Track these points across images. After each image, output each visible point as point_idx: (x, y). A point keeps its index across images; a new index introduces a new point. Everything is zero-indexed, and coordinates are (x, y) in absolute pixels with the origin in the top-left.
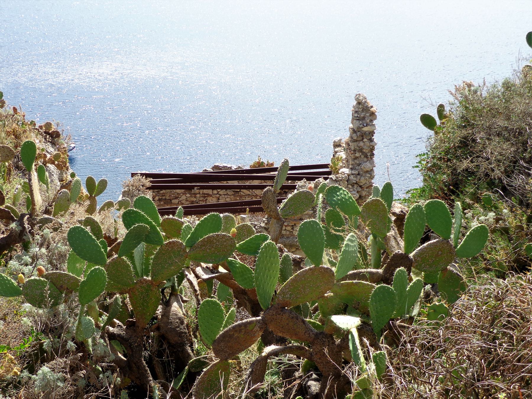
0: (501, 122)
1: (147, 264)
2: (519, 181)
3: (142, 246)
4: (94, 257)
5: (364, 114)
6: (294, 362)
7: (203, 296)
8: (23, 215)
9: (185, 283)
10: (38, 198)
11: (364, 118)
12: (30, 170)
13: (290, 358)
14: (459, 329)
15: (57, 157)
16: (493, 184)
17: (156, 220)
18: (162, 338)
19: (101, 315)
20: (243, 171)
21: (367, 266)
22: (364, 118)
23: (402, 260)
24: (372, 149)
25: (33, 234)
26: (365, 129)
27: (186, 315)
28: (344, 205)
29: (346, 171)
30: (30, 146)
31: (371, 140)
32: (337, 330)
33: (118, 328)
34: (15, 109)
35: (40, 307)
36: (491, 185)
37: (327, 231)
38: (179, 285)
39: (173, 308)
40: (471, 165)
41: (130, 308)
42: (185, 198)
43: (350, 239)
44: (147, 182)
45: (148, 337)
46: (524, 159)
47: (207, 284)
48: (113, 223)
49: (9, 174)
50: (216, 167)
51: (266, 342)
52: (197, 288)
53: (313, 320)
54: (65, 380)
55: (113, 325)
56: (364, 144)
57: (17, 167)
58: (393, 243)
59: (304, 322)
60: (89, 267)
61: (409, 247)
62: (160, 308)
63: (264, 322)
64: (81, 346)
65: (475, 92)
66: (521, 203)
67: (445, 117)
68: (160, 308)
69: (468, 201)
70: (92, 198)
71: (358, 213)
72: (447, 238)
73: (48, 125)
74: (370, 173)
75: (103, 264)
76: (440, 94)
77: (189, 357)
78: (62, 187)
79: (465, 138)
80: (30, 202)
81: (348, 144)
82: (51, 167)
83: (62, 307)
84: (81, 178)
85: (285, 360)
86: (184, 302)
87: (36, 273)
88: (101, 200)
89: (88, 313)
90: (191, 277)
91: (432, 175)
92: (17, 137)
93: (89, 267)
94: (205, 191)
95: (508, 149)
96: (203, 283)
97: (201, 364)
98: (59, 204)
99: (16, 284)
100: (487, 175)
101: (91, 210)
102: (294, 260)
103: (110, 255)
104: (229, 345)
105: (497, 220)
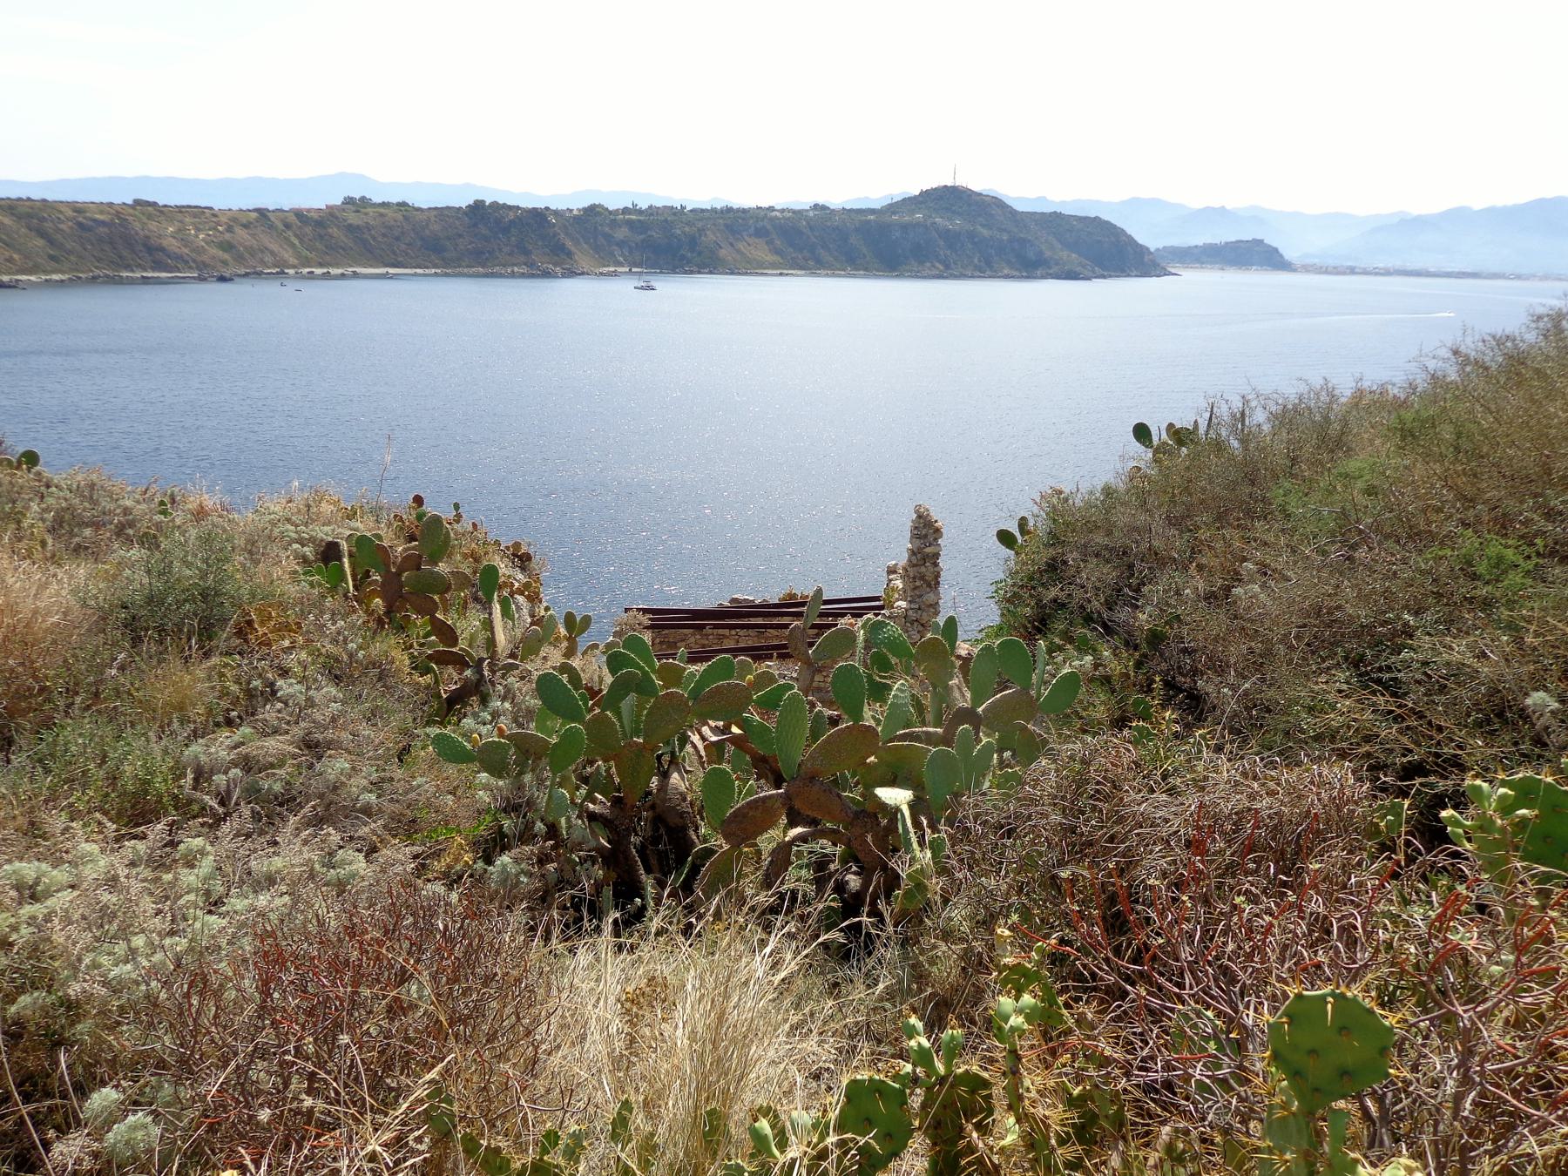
0: (1100, 539)
1: (637, 722)
2: (1122, 614)
3: (631, 698)
4: (572, 714)
5: (926, 531)
6: (828, 851)
7: (709, 763)
8: (481, 660)
9: (689, 748)
10: (501, 638)
11: (926, 536)
12: (490, 601)
13: (825, 846)
14: (1034, 801)
15: (527, 586)
16: (1092, 619)
17: (651, 665)
18: (658, 820)
19: (578, 788)
20: (769, 606)
21: (924, 724)
22: (926, 536)
23: (968, 715)
24: (938, 576)
25: (493, 685)
26: (928, 550)
27: (690, 789)
28: (895, 645)
29: (903, 604)
30: (492, 571)
31: (936, 565)
32: (883, 806)
33: (600, 805)
34: (474, 525)
35: (500, 777)
36: (1088, 620)
37: (869, 677)
38: (681, 750)
39: (672, 781)
40: (1062, 595)
41: (617, 780)
42: (694, 640)
43: (899, 687)
44: (645, 620)
45: (640, 819)
46: (1129, 586)
47: (716, 750)
48: (595, 669)
49: (465, 607)
50: (734, 600)
51: (792, 824)
52: (703, 753)
53: (855, 795)
54: (531, 875)
55: (594, 801)
56: (927, 570)
57: (476, 599)
58: (957, 694)
59: (839, 796)
60: (563, 725)
61: (977, 700)
62: (654, 779)
63: (787, 797)
64: (552, 831)
65: (1066, 500)
66: (1127, 644)
67: (1029, 532)
68: (654, 779)
69: (1057, 640)
70: (571, 640)
71: (911, 655)
72: (1026, 688)
73: (517, 545)
74: (934, 607)
75: (581, 721)
76: (1022, 501)
77: (693, 845)
78: (532, 624)
79: (1053, 559)
80: (491, 643)
81: (905, 569)
82: (520, 599)
83: (527, 778)
84: (558, 613)
85: (817, 848)
86: (687, 772)
87: (496, 732)
88: (583, 642)
89: (561, 785)
90: (695, 738)
91: (1012, 608)
92: (477, 560)
93: (563, 725)
94: (721, 631)
95: (1110, 573)
96: (710, 746)
97: (709, 852)
98: (528, 647)
99: (469, 747)
100: (1082, 607)
101: (570, 653)
102: (830, 718)
103: (591, 710)
104: (744, 827)
105: (1096, 666)
